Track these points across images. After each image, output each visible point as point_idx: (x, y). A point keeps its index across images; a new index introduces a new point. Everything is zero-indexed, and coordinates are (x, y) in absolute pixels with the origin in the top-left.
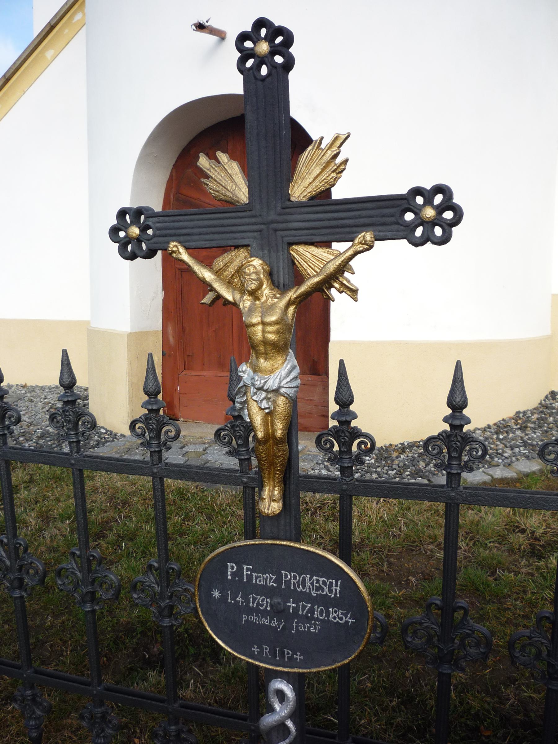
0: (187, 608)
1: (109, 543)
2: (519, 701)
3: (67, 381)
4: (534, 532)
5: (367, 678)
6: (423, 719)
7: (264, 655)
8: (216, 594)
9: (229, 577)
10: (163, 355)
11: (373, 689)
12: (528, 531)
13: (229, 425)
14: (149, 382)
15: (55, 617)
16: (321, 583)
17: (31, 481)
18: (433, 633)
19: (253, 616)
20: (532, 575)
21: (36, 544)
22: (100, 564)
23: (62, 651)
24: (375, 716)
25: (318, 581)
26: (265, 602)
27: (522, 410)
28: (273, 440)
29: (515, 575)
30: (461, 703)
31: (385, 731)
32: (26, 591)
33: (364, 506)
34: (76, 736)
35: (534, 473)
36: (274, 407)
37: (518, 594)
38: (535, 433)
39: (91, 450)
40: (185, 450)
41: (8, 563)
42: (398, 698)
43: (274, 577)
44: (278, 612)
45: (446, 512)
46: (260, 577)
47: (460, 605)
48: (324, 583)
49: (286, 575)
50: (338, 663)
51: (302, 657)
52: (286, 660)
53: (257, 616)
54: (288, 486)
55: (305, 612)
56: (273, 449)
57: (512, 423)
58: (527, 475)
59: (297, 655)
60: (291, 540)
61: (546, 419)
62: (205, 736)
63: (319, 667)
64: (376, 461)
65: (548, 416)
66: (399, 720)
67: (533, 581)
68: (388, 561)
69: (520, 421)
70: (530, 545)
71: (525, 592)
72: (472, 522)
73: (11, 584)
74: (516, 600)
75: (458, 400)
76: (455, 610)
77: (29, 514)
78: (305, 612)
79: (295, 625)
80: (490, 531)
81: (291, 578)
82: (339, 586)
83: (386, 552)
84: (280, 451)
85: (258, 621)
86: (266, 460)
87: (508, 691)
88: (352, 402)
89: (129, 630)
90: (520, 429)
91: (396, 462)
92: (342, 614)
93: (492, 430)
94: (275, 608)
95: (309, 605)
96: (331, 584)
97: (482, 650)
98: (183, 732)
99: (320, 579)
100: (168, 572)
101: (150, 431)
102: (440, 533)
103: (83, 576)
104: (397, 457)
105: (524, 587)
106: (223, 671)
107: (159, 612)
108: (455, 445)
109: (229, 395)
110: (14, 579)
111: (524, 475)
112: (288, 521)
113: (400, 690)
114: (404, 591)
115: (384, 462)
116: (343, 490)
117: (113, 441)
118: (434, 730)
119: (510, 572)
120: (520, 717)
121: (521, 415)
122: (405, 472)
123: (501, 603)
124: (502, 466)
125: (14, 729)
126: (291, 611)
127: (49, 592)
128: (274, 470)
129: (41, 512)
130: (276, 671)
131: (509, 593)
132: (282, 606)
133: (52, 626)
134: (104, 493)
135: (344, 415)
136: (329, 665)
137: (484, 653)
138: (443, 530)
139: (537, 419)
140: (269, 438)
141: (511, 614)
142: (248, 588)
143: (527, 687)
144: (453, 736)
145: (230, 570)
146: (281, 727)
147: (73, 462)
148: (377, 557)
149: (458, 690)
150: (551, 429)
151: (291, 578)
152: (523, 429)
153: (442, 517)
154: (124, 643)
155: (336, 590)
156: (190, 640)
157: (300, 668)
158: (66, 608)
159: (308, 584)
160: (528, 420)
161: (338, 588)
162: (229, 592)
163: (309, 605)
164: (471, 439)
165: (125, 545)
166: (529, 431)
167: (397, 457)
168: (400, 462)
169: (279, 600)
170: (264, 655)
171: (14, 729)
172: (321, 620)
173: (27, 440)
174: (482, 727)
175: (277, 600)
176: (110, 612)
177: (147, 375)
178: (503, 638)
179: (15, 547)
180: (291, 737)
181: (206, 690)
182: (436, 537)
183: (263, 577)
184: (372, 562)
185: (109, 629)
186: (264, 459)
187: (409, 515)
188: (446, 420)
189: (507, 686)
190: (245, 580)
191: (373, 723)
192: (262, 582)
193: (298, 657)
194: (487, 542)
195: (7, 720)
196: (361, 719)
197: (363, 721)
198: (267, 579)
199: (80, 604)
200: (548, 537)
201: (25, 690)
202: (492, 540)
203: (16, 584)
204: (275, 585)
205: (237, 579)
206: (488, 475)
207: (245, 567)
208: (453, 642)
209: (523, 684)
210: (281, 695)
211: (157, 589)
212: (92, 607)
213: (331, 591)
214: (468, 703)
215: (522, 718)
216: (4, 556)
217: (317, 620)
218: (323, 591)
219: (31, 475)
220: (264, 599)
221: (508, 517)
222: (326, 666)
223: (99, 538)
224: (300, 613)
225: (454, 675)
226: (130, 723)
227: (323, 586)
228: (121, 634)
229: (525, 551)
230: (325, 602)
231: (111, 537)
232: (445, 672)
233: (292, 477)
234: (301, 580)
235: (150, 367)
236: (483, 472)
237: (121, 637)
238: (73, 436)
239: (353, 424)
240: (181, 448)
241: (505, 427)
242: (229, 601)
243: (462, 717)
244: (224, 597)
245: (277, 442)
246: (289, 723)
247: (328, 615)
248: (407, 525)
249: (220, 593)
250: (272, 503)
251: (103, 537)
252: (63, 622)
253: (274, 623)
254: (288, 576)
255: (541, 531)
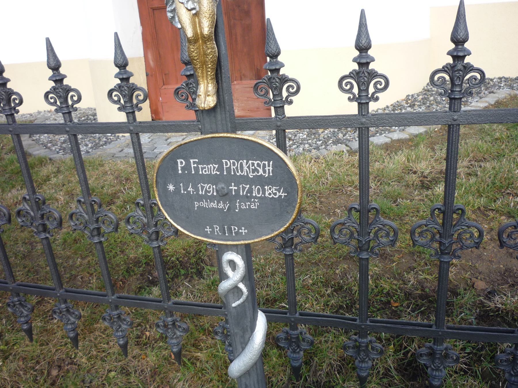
0: (168, 232)
1: (117, 207)
2: (417, 282)
3: (53, 64)
4: (423, 173)
5: (309, 277)
6: (350, 299)
7: (216, 234)
8: (171, 187)
9: (180, 172)
10: (147, 75)
11: (314, 284)
12: (419, 172)
13: (184, 84)
14: (117, 56)
15: (83, 258)
16: (256, 165)
17: (59, 171)
18: (354, 230)
19: (203, 202)
20: (423, 200)
21: (65, 212)
22: (100, 206)
23: (90, 280)
24: (316, 301)
25: (253, 164)
26: (211, 189)
27: (410, 94)
28: (202, 40)
29: (411, 201)
30: (376, 287)
31: (324, 310)
32: (49, 233)
33: (300, 166)
34: (104, 334)
35: (421, 134)
36: (200, 8)
37: (413, 213)
38: (421, 108)
39: (101, 147)
40: (169, 141)
41: (32, 214)
42: (332, 288)
43: (216, 166)
44: (224, 196)
45: (360, 165)
46: (205, 168)
47: (373, 207)
48: (259, 165)
49: (226, 162)
50: (276, 231)
51: (246, 231)
52: (234, 235)
53: (206, 201)
54: (220, 85)
55: (245, 193)
56: (203, 48)
57: (404, 103)
58: (416, 136)
59: (242, 230)
60: (228, 132)
61: (429, 98)
62: (196, 326)
63: (261, 237)
64: (307, 136)
65: (429, 96)
66: (333, 301)
67: (424, 204)
68: (320, 201)
69: (409, 102)
70: (421, 181)
71: (418, 211)
72: (378, 170)
73: (37, 229)
74: (412, 217)
75: (363, 42)
76: (369, 211)
77: (59, 193)
78: (245, 193)
79: (238, 204)
80: (391, 174)
81: (230, 165)
82: (271, 166)
83: (318, 195)
84: (209, 49)
85: (208, 206)
86: (197, 59)
87: (409, 276)
88: (279, 53)
89: (137, 262)
90: (410, 106)
91: (322, 135)
92: (276, 190)
93: (390, 109)
94: (220, 192)
95: (248, 186)
96: (264, 165)
97: (391, 239)
98: (177, 321)
99: (254, 162)
100: (151, 207)
101: (124, 96)
102: (356, 179)
103: (89, 217)
104: (322, 133)
105: (418, 208)
106: (205, 282)
107: (149, 238)
108: (363, 80)
109: (182, 60)
110: (39, 225)
111: (414, 136)
112: (224, 116)
113: (333, 283)
114: (332, 218)
115: (313, 137)
116: (278, 126)
117: (117, 140)
118: (358, 306)
119: (407, 199)
120: (419, 292)
121: (410, 97)
122: (328, 141)
123: (402, 220)
124: (398, 131)
125: (59, 334)
126: (234, 193)
127: (77, 243)
128: (207, 68)
129: (68, 192)
130: (227, 245)
131: (407, 213)
132: (226, 190)
133: (81, 265)
134: (112, 174)
135: (273, 65)
136: (269, 234)
137: (392, 241)
138: (358, 177)
139: (422, 99)
140: (199, 39)
141: (409, 226)
142: (197, 179)
143: (423, 272)
144: (372, 308)
145: (179, 165)
146: (235, 289)
147: (68, 129)
148: (312, 199)
149: (374, 278)
150: (432, 104)
151: (230, 165)
152: (412, 106)
153: (357, 168)
154: (133, 271)
155: (269, 170)
156: (181, 265)
157: (246, 240)
158: (90, 252)
159: (245, 168)
160: (415, 100)
161: (271, 168)
162: (181, 185)
163: (248, 186)
164: (375, 74)
165: (130, 207)
166: (416, 107)
167: (322, 133)
168: (325, 135)
169: (223, 186)
170: (216, 234)
171: (59, 334)
172: (259, 197)
173: (54, 145)
174: (392, 301)
175: (221, 185)
176: (122, 252)
177: (116, 51)
178: (404, 242)
179: (36, 202)
180: (244, 297)
181: (195, 296)
182: (353, 182)
183: (208, 167)
184: (309, 202)
185: (122, 263)
186: (196, 58)
187: (334, 169)
188: (354, 60)
189: (408, 273)
190: (193, 172)
191: (314, 306)
192: (207, 172)
193: (243, 231)
194: (390, 182)
195: (53, 329)
196: (305, 304)
197: (307, 305)
198: (211, 169)
199: (90, 238)
200: (433, 175)
201: (61, 305)
202: (394, 180)
203: (41, 228)
204: (218, 173)
205: (186, 172)
206: (388, 138)
207: (192, 161)
208: (369, 235)
209: (420, 270)
210: (233, 264)
211: (145, 220)
212: (99, 239)
213: (264, 171)
214: (381, 286)
215: (420, 292)
216: (29, 209)
217: (256, 197)
218: (258, 172)
219: (58, 167)
220: (210, 186)
221: (404, 164)
222: (266, 235)
223: (110, 205)
224: (241, 194)
225: (371, 269)
226: (142, 322)
227: (258, 168)
228: (131, 266)
229: (417, 186)
230: (261, 181)
231: (119, 202)
232: (364, 257)
233: (223, 76)
234: (239, 166)
235: (117, 43)
236: (385, 136)
237: (131, 267)
238: (65, 109)
239: (282, 72)
240: (166, 140)
241: (399, 106)
242: (182, 192)
243: (377, 296)
244: (177, 190)
245: (205, 39)
246: (241, 286)
247: (264, 193)
248: (332, 175)
249: (174, 186)
250: (207, 98)
251: (114, 203)
252: (89, 262)
253: (221, 205)
254: (227, 163)
255: (428, 171)
